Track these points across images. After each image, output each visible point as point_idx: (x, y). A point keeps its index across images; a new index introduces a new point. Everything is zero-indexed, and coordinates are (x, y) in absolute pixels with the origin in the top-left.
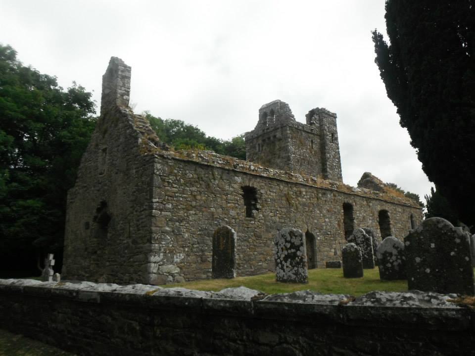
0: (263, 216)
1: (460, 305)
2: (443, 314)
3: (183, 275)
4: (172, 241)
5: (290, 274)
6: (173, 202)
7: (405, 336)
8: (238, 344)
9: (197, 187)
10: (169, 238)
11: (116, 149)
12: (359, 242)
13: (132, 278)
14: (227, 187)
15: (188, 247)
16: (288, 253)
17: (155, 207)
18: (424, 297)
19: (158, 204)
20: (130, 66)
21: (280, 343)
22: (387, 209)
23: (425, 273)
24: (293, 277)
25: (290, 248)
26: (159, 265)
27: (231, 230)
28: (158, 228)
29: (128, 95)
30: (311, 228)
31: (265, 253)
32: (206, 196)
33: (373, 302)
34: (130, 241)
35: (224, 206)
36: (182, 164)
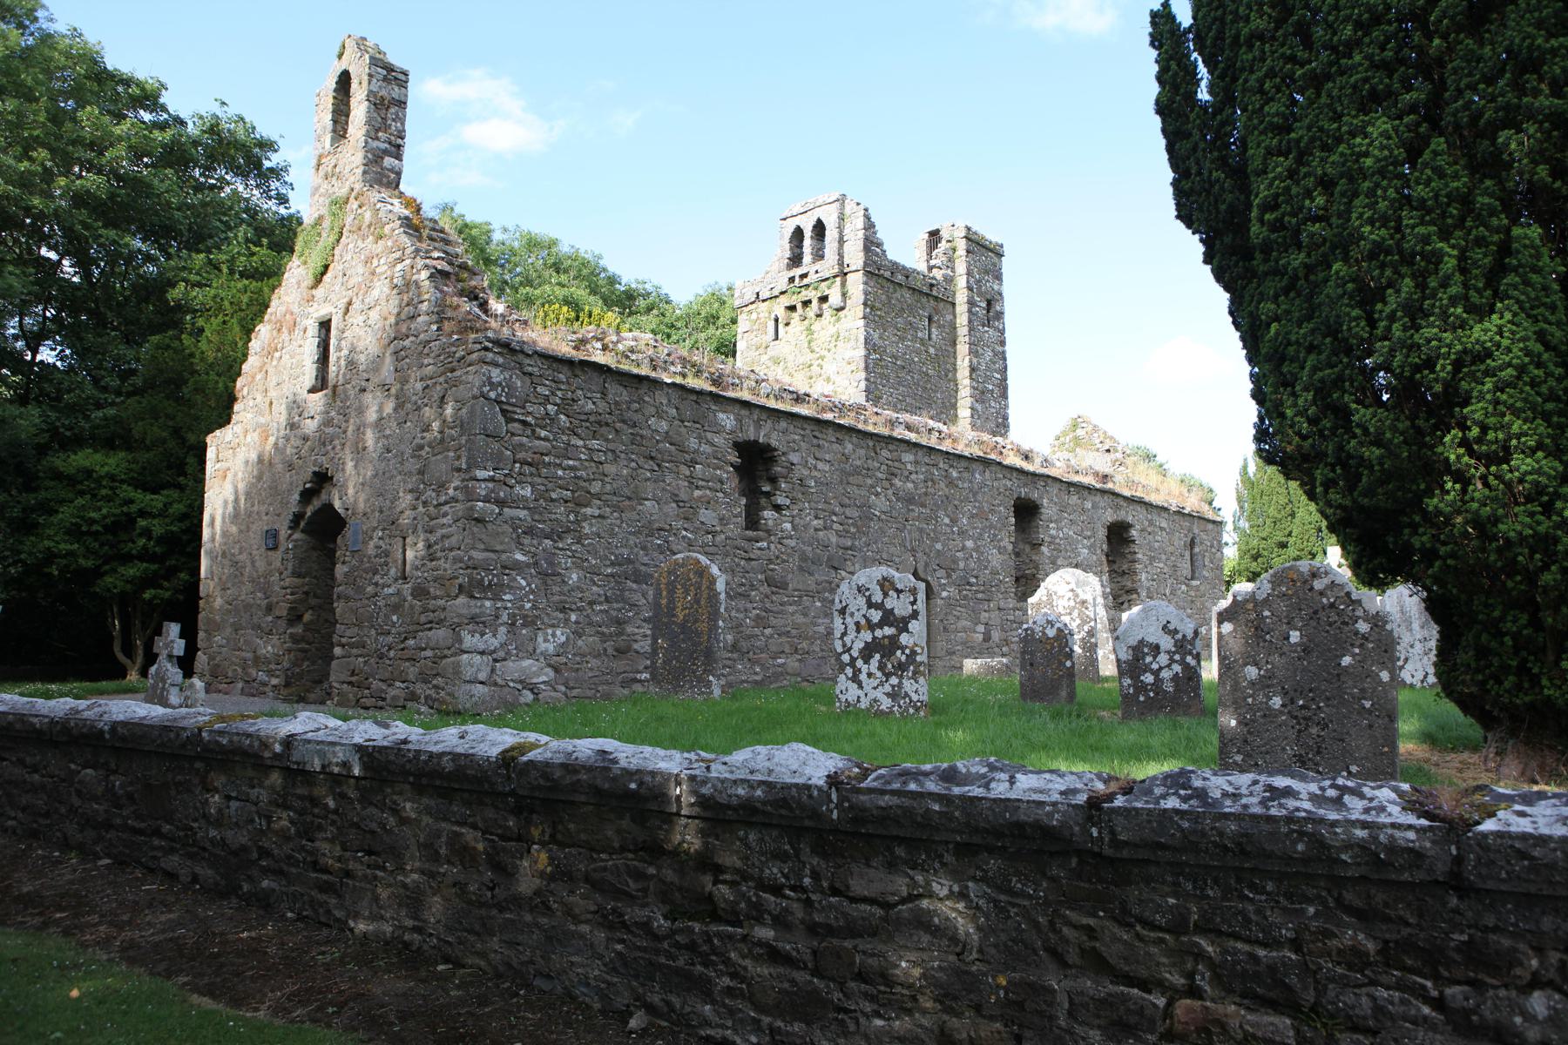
0: (794, 528)
2: (1382, 838)
4: (532, 592)
5: (879, 694)
6: (539, 480)
7: (1270, 887)
8: (788, 898)
9: (607, 440)
10: (524, 583)
11: (362, 318)
14: (693, 443)
15: (578, 609)
16: (874, 638)
18: (1323, 789)
19: (491, 485)
20: (405, 68)
21: (911, 898)
22: (1130, 519)
23: (1269, 708)
24: (886, 703)
25: (881, 625)
26: (496, 661)
27: (707, 567)
28: (492, 555)
29: (399, 157)
30: (927, 565)
31: (794, 632)
32: (633, 465)
33: (1185, 799)
34: (407, 588)
35: (683, 496)
36: (565, 369)
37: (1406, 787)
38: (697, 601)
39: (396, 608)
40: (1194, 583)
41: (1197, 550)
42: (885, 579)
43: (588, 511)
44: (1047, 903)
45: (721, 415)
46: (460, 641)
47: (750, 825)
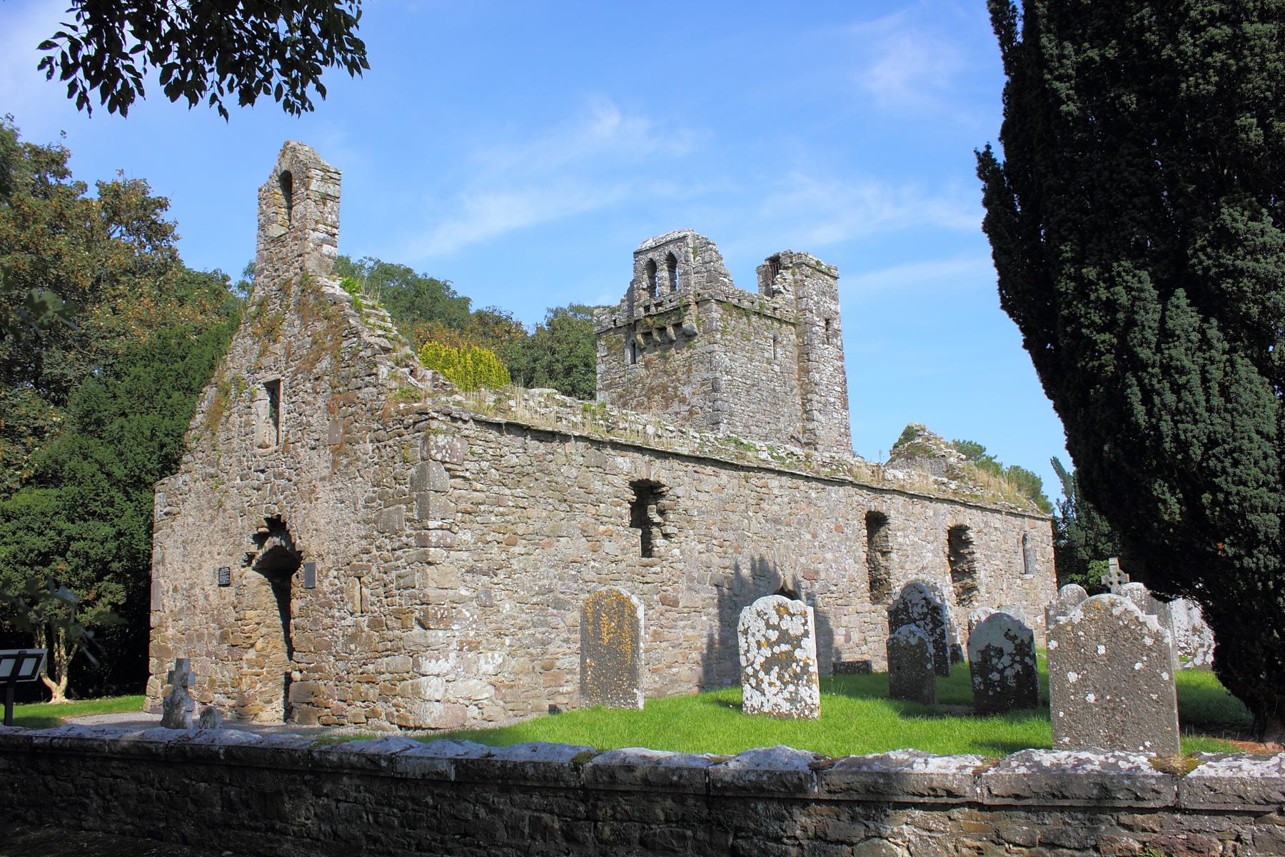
1: (1163, 770)
3: (502, 703)
10: (468, 615)
12: (916, 615)
13: (373, 711)
14: (597, 486)
16: (773, 654)
17: (434, 540)
19: (440, 532)
22: (967, 523)
24: (786, 707)
25: (778, 643)
34: (364, 621)
37: (1154, 754)
38: (620, 627)
39: (352, 638)
40: (1027, 576)
41: (1028, 546)
42: (779, 605)
43: (516, 550)
44: (952, 835)
45: (620, 460)
46: (419, 666)
47: (758, 799)
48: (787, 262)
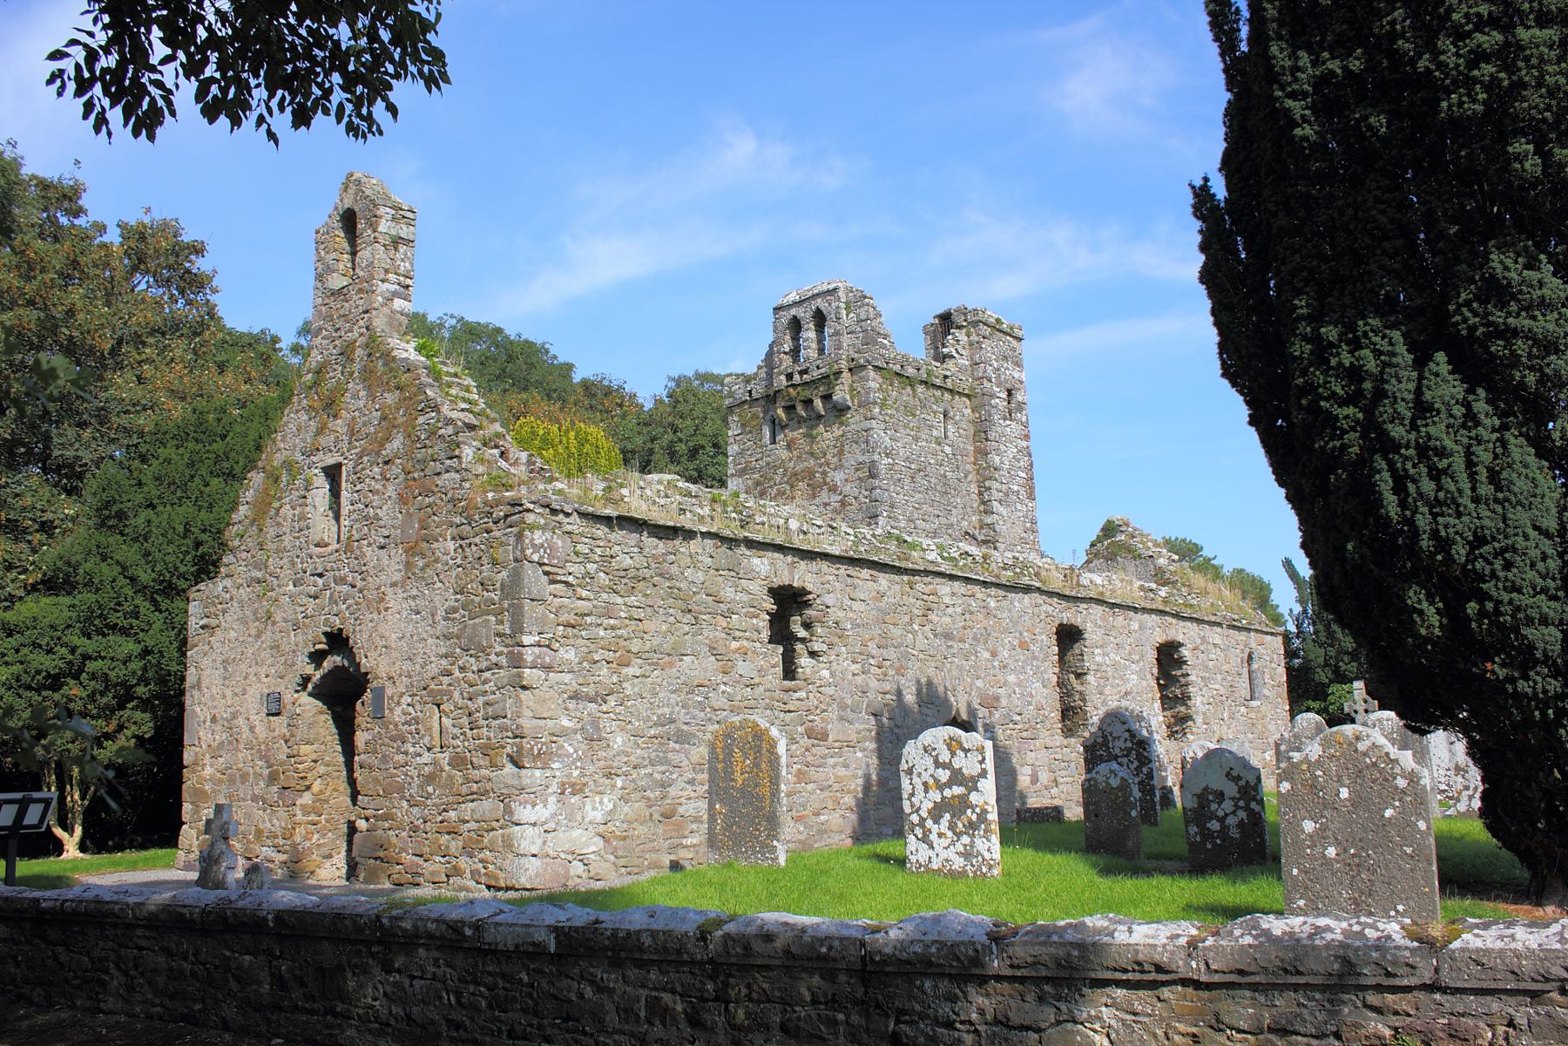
1: (1420, 940)
3: (612, 858)
10: (571, 750)
12: (1117, 751)
13: (455, 868)
14: (728, 593)
16: (943, 798)
17: (529, 659)
19: (537, 650)
22: (1180, 638)
24: (959, 863)
25: (949, 784)
34: (444, 758)
37: (1408, 921)
38: (757, 765)
39: (430, 779)
40: (1254, 704)
41: (1255, 666)
42: (951, 738)
43: (630, 671)
44: (1162, 1019)
45: (756, 561)
46: (511, 813)
47: (925, 975)
48: (960, 320)
